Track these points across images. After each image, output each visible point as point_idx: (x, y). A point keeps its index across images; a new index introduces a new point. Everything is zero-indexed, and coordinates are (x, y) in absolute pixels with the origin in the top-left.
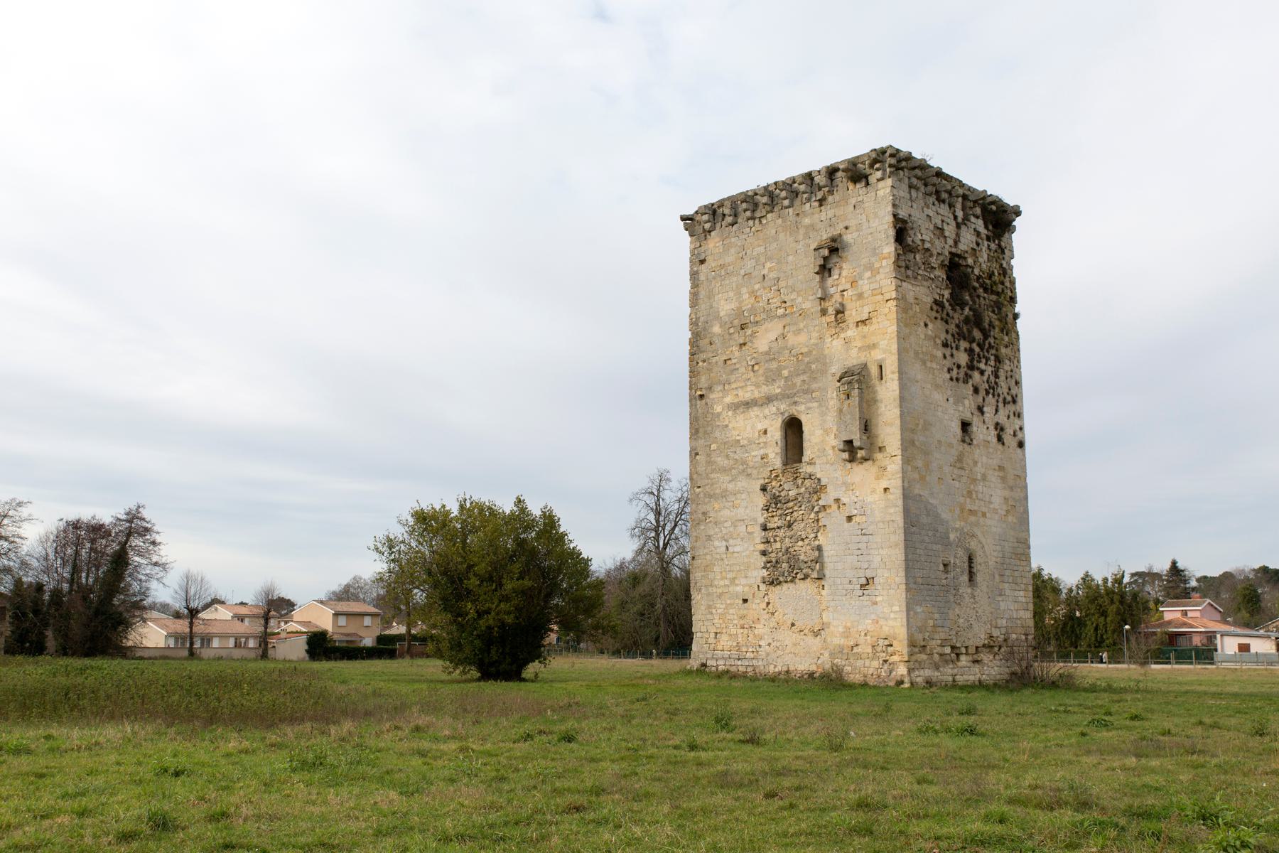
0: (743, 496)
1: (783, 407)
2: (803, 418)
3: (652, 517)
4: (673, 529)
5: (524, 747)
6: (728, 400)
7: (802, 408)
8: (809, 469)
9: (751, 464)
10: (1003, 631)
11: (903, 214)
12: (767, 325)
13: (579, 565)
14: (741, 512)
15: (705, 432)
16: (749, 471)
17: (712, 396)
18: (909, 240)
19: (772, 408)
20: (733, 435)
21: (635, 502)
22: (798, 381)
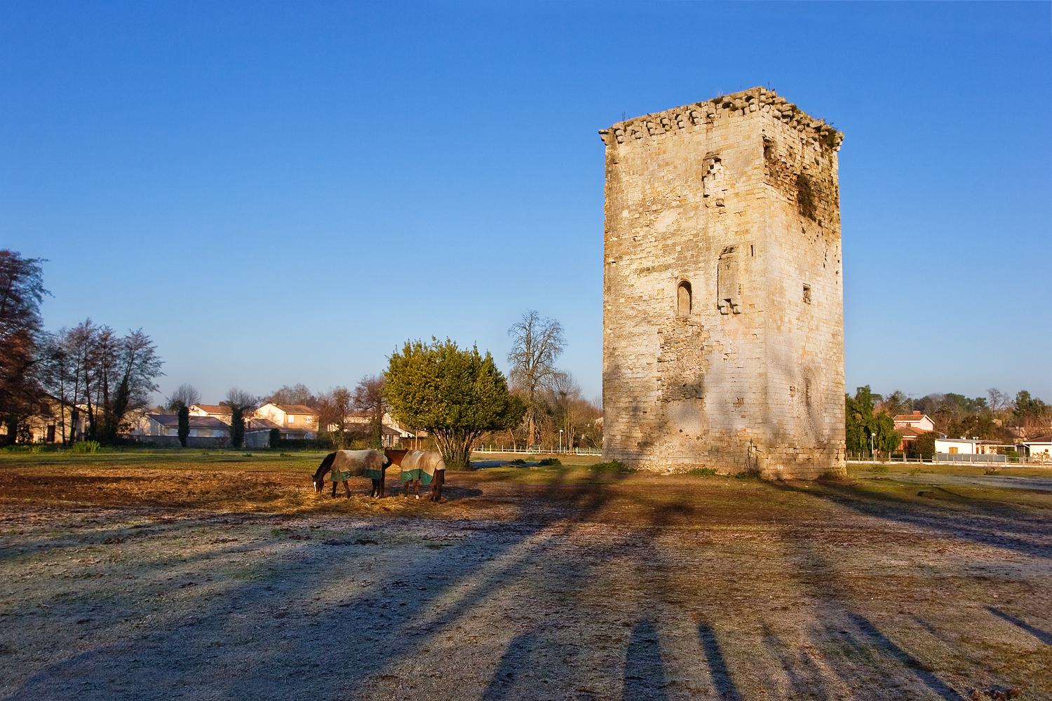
0: (645, 337)
1: (676, 274)
2: (691, 281)
3: (523, 346)
4: (540, 356)
5: (846, 631)
6: (634, 266)
7: (691, 274)
8: (696, 319)
9: (651, 314)
10: (827, 437)
11: (769, 135)
12: (665, 213)
13: (34, 324)
14: (642, 350)
15: (616, 290)
16: (650, 319)
17: (621, 263)
18: (772, 156)
19: (668, 274)
20: (637, 292)
21: (511, 334)
22: (689, 254)
